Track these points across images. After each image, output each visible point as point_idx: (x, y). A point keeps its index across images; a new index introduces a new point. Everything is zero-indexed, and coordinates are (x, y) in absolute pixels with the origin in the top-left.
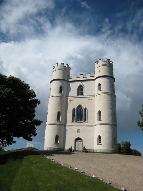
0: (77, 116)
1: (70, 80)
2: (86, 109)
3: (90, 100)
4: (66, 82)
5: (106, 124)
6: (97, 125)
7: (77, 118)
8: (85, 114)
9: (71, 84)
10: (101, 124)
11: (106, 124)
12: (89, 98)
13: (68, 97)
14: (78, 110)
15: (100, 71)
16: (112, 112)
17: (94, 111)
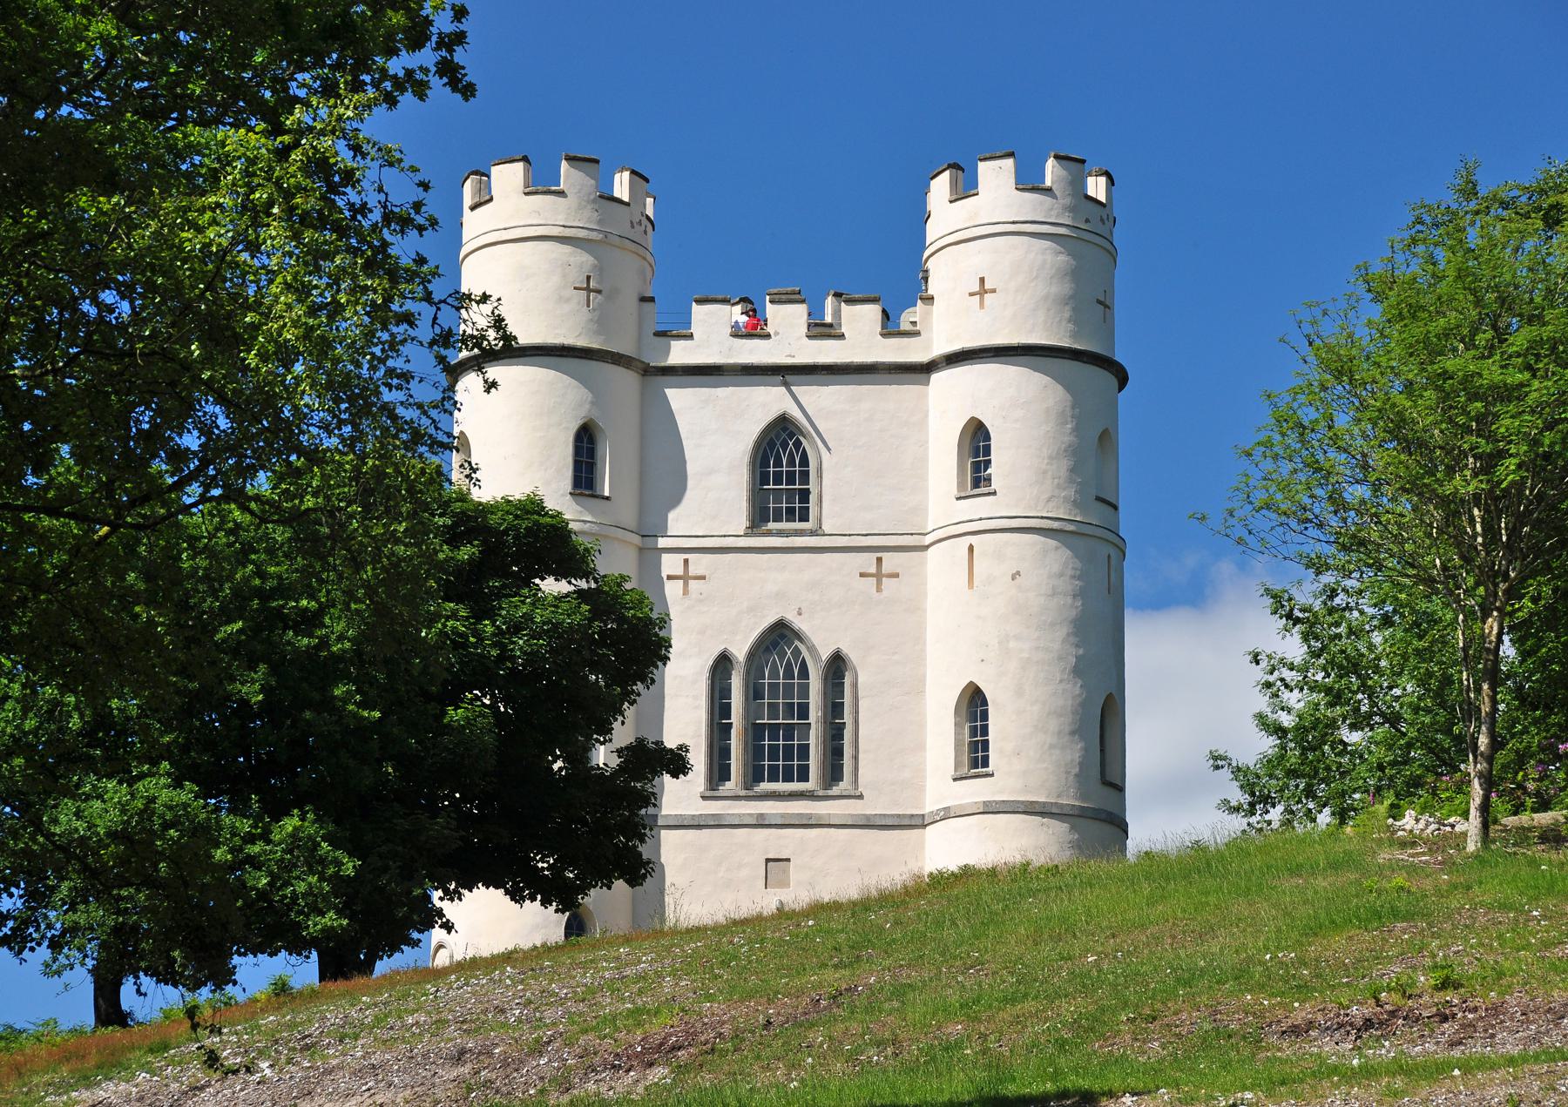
0: (755, 732)
1: (680, 354)
2: (837, 666)
3: (879, 576)
4: (626, 380)
5: (1030, 809)
6: (947, 814)
7: (754, 751)
8: (834, 708)
9: (680, 399)
10: (990, 809)
11: (1030, 809)
12: (867, 561)
13: (662, 543)
14: (765, 463)
15: (983, 290)
16: (1083, 705)
17: (917, 688)
